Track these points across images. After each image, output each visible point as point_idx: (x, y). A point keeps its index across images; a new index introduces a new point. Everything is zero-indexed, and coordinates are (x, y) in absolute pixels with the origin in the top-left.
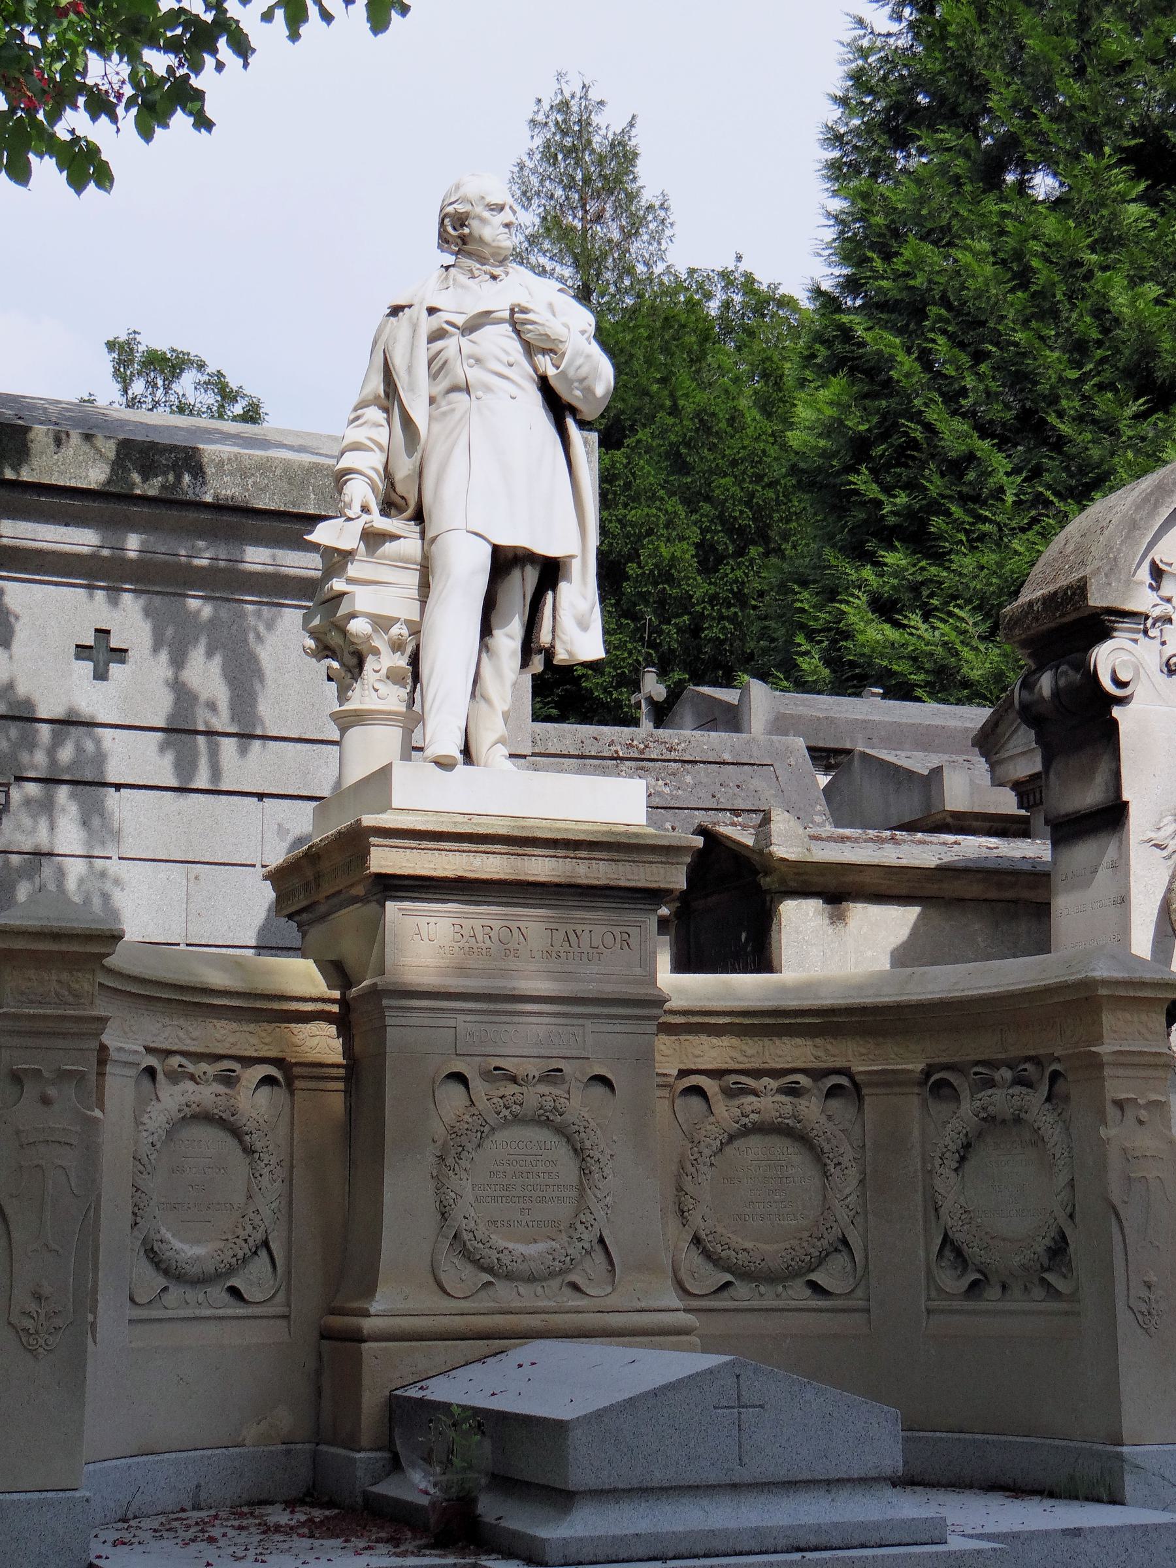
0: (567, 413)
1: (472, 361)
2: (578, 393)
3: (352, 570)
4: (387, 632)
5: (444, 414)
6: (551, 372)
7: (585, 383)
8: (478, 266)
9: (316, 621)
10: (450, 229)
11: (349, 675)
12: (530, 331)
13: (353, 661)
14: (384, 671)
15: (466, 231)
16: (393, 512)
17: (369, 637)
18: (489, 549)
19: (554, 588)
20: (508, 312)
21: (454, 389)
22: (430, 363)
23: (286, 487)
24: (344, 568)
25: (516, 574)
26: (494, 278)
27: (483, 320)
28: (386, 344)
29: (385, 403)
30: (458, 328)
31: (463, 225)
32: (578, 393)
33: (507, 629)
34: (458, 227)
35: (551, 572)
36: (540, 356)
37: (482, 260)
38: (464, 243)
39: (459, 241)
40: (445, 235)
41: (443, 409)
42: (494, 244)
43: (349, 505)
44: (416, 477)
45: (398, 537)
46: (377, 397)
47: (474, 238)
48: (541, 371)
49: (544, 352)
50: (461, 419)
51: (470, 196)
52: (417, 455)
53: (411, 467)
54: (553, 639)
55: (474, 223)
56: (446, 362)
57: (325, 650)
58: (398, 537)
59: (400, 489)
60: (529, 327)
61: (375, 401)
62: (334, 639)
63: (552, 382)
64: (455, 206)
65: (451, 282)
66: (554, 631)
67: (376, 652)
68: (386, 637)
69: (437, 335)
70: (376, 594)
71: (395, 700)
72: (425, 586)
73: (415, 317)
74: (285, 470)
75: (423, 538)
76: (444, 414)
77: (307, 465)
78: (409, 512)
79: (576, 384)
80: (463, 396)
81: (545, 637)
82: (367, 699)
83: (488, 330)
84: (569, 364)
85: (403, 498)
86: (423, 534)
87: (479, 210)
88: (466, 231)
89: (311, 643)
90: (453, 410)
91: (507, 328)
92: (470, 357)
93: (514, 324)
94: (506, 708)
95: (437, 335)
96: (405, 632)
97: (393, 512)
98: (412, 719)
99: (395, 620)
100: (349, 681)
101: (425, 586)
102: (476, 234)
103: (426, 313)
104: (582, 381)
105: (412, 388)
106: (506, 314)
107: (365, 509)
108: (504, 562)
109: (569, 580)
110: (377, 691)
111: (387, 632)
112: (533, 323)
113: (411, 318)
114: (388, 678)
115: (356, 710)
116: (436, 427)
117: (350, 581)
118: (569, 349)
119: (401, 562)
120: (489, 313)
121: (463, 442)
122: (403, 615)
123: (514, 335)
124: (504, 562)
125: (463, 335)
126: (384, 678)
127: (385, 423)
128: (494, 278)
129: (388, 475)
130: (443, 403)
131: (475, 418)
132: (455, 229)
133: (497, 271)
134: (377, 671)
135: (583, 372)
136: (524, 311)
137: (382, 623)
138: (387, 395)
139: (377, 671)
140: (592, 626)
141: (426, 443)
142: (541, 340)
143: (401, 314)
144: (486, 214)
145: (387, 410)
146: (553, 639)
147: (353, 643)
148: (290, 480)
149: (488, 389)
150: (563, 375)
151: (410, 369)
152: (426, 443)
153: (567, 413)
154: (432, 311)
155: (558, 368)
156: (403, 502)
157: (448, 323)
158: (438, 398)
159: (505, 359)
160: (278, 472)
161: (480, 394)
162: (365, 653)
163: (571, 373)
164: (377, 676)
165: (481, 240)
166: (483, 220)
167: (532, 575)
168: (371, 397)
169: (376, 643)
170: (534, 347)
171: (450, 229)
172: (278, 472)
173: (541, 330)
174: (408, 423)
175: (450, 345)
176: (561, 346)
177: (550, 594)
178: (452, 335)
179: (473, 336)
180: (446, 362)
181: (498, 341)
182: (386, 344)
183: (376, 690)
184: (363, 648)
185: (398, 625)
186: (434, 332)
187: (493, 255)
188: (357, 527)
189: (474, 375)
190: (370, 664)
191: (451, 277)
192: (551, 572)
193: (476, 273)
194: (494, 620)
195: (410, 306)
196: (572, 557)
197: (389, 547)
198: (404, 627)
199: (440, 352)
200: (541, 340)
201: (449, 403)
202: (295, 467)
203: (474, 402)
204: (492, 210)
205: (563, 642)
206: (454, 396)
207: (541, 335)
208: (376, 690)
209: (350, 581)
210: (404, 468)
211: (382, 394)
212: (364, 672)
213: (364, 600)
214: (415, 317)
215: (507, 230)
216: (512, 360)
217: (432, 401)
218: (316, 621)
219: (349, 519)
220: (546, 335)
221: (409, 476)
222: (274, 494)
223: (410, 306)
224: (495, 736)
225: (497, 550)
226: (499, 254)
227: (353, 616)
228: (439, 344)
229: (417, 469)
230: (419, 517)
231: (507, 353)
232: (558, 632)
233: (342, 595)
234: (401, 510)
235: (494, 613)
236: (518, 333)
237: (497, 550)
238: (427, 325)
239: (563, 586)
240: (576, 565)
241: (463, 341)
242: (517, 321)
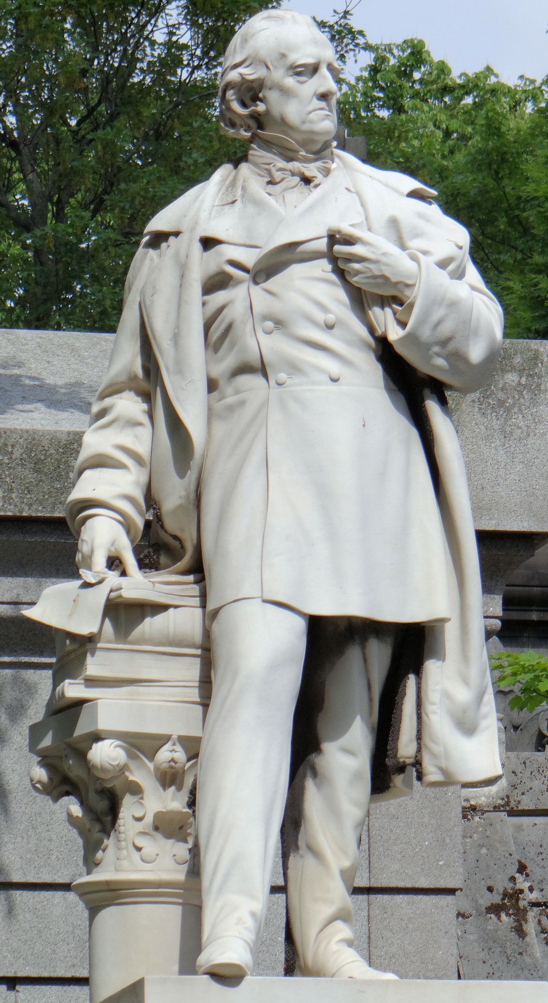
0: (427, 392)
1: (269, 324)
2: (440, 362)
3: (94, 666)
4: (151, 757)
5: (231, 408)
6: (394, 334)
7: (451, 346)
8: (281, 163)
9: (47, 741)
10: (236, 106)
11: (97, 827)
12: (358, 273)
13: (102, 805)
14: (149, 819)
15: (261, 107)
16: (163, 559)
17: (123, 769)
18: (301, 625)
19: (418, 671)
20: (325, 240)
21: (244, 369)
22: (207, 327)
23: (31, 477)
24: (81, 662)
25: (353, 655)
26: (307, 181)
27: (287, 256)
28: (143, 293)
29: (145, 386)
30: (246, 270)
31: (256, 99)
32: (440, 362)
33: (344, 741)
34: (248, 102)
35: (412, 645)
36: (377, 310)
37: (289, 155)
38: (261, 126)
39: (252, 123)
40: (228, 115)
41: (230, 400)
42: (305, 127)
43: (88, 564)
44: (192, 507)
45: (165, 608)
46: (133, 378)
47: (274, 120)
48: (379, 332)
49: (384, 301)
50: (254, 418)
51: (263, 53)
52: (192, 475)
53: (183, 493)
54: (419, 750)
55: (272, 96)
56: (229, 328)
57: (61, 784)
58: (165, 608)
59: (170, 524)
60: (356, 266)
61: (128, 384)
62: (71, 766)
63: (399, 349)
64: (241, 70)
65: (239, 192)
66: (419, 737)
67: (136, 790)
68: (151, 766)
69: (216, 283)
70: (130, 701)
71: (168, 862)
72: (206, 684)
73: (183, 253)
74: (29, 450)
75: (203, 605)
76: (231, 408)
77: (64, 438)
78: (185, 562)
79: (436, 349)
80: (256, 380)
81: (405, 747)
82: (125, 863)
83: (296, 271)
84: (421, 322)
85: (176, 537)
86: (204, 596)
87: (279, 75)
88: (261, 107)
89: (41, 774)
90: (242, 403)
91: (323, 267)
92: (266, 318)
93: (334, 259)
94: (347, 863)
95: (216, 283)
96: (180, 755)
97: (449, 211)
98: (190, 895)
99: (162, 740)
100: (97, 835)
101: (206, 684)
102: (276, 112)
103: (198, 246)
104: (444, 343)
105: (180, 369)
106: (322, 245)
107: (114, 562)
108: (327, 639)
109: (442, 658)
110: (138, 854)
111: (151, 757)
112: (361, 259)
113: (177, 254)
114: (156, 828)
115: (107, 883)
116: (219, 429)
117: (91, 682)
118: (419, 297)
119: (172, 646)
120: (293, 246)
121: (256, 457)
122: (176, 729)
123: (334, 277)
124: (327, 639)
125: (256, 283)
126: (150, 829)
127: (145, 419)
128: (307, 181)
129: (150, 499)
130: (229, 390)
131: (275, 417)
132: (244, 105)
133: (311, 170)
134: (139, 819)
135: (446, 329)
136: (349, 241)
137: (142, 745)
138: (147, 371)
139: (139, 819)
140: (484, 724)
141: (204, 456)
142: (377, 285)
143: (164, 245)
144: (290, 81)
145: (147, 397)
146: (419, 750)
147: (98, 779)
148: (38, 466)
149: (294, 368)
150: (412, 339)
151: (176, 338)
152: (204, 456)
153: (427, 392)
154: (208, 243)
155: (403, 325)
156: (176, 543)
157: (234, 263)
158: (222, 383)
159: (321, 317)
160: (17, 454)
161: (282, 376)
162: (119, 791)
163: (426, 334)
164: (139, 826)
165: (283, 123)
166: (285, 92)
167: (379, 655)
168: (123, 378)
169: (136, 776)
170: (369, 293)
171: (236, 106)
172: (17, 454)
173: (375, 269)
174: (176, 426)
175: (239, 298)
176: (407, 292)
177: (411, 680)
178: (239, 282)
179: (274, 283)
180: (229, 328)
181: (311, 288)
182: (143, 293)
183: (139, 849)
184: (117, 784)
185: (170, 743)
186: (211, 278)
187: (304, 144)
188: (98, 598)
189: (271, 345)
190: (128, 809)
191: (240, 183)
192: (412, 645)
193: (278, 176)
194: (323, 725)
195: (177, 234)
196: (443, 621)
197: (151, 625)
198: (178, 748)
199: (221, 310)
200: (377, 285)
201: (237, 392)
202: (45, 443)
203: (275, 390)
204: (299, 74)
205: (434, 755)
206: (245, 380)
207: (375, 277)
208: (139, 849)
209: (91, 682)
210: (174, 494)
211: (140, 372)
212: (120, 822)
213: (111, 711)
214: (183, 253)
215: (323, 104)
216: (331, 318)
217: (212, 385)
218: (47, 741)
219: (87, 585)
220: (384, 277)
221: (180, 507)
222: (11, 490)
223: (177, 234)
224: (328, 911)
225: (317, 626)
226: (313, 141)
227: (97, 737)
228: (220, 297)
229: (192, 496)
230: (198, 569)
231: (324, 308)
232: (426, 739)
233: (80, 703)
234: (175, 555)
235: (321, 715)
236: (341, 273)
237: (317, 626)
238: (201, 265)
239: (431, 667)
240: (451, 635)
241: (257, 291)
242: (338, 252)
